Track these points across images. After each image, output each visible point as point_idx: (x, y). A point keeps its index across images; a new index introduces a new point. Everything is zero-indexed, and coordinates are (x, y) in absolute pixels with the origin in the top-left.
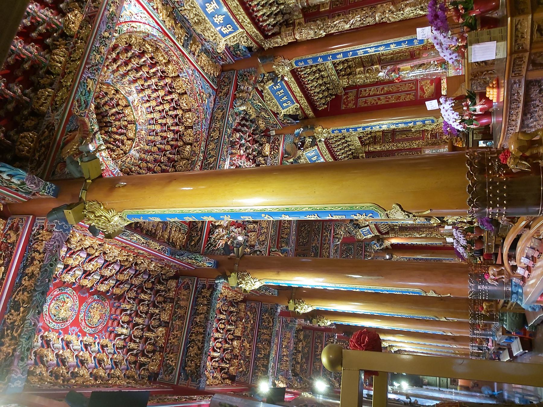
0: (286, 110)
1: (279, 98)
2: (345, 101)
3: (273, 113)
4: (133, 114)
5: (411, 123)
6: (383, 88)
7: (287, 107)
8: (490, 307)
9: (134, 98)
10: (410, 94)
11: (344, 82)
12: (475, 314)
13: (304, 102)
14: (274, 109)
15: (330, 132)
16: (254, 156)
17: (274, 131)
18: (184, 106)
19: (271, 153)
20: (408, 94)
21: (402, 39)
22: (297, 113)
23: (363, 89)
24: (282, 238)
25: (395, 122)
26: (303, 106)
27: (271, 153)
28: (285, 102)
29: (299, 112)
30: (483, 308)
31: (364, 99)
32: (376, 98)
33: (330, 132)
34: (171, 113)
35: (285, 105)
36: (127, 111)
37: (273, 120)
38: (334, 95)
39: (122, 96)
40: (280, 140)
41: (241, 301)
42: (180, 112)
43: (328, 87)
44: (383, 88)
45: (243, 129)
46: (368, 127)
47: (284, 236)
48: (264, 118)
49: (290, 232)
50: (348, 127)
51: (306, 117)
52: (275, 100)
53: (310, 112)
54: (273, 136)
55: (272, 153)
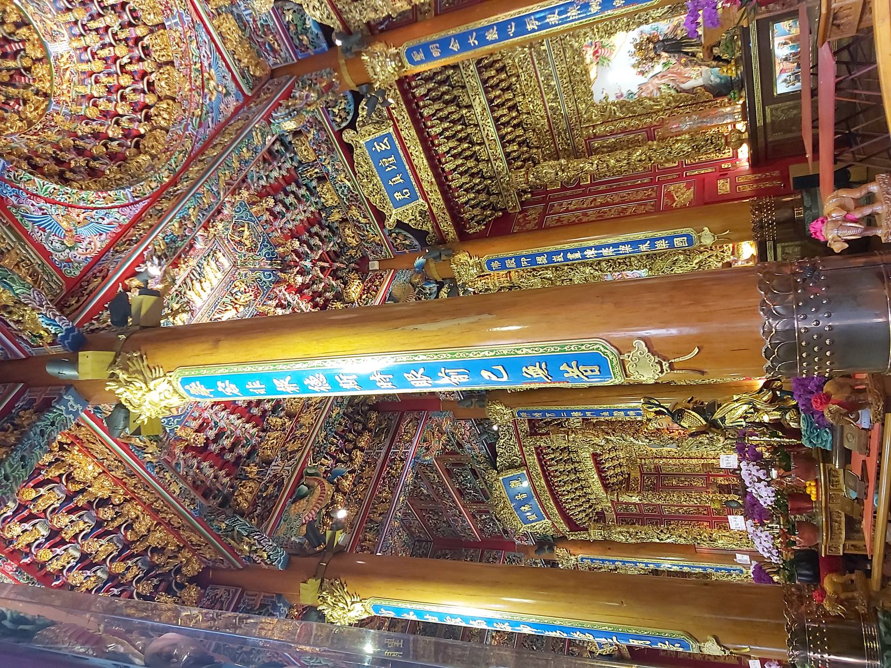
0: (400, 210)
1: (386, 177)
2: (521, 220)
3: (374, 208)
4: (51, 81)
5: (643, 242)
6: (595, 200)
7: (380, 140)
8: (847, 587)
9: (61, 47)
10: (645, 204)
11: (520, 179)
12: (803, 630)
13: (436, 197)
14: (375, 200)
15: (579, 559)
16: (327, 301)
17: (377, 263)
18: (162, 87)
19: (360, 298)
20: (641, 205)
21: (659, 234)
22: (425, 228)
23: (556, 204)
24: (371, 521)
25: (611, 241)
26: (435, 210)
27: (360, 298)
28: (399, 188)
29: (428, 227)
30: (823, 593)
31: (556, 217)
32: (578, 213)
33: (579, 559)
34: (93, 25)
35: (398, 196)
36: (40, 70)
37: (375, 233)
38: (501, 210)
39: (36, 36)
40: (385, 276)
41: (192, 580)
42: (150, 99)
43: (486, 185)
44: (595, 200)
45: (312, 242)
46: (557, 253)
47: (375, 517)
48: (357, 226)
49: (389, 510)
50: (519, 253)
51: (442, 239)
52: (377, 179)
53: (448, 227)
54: (374, 271)
55: (364, 297)
